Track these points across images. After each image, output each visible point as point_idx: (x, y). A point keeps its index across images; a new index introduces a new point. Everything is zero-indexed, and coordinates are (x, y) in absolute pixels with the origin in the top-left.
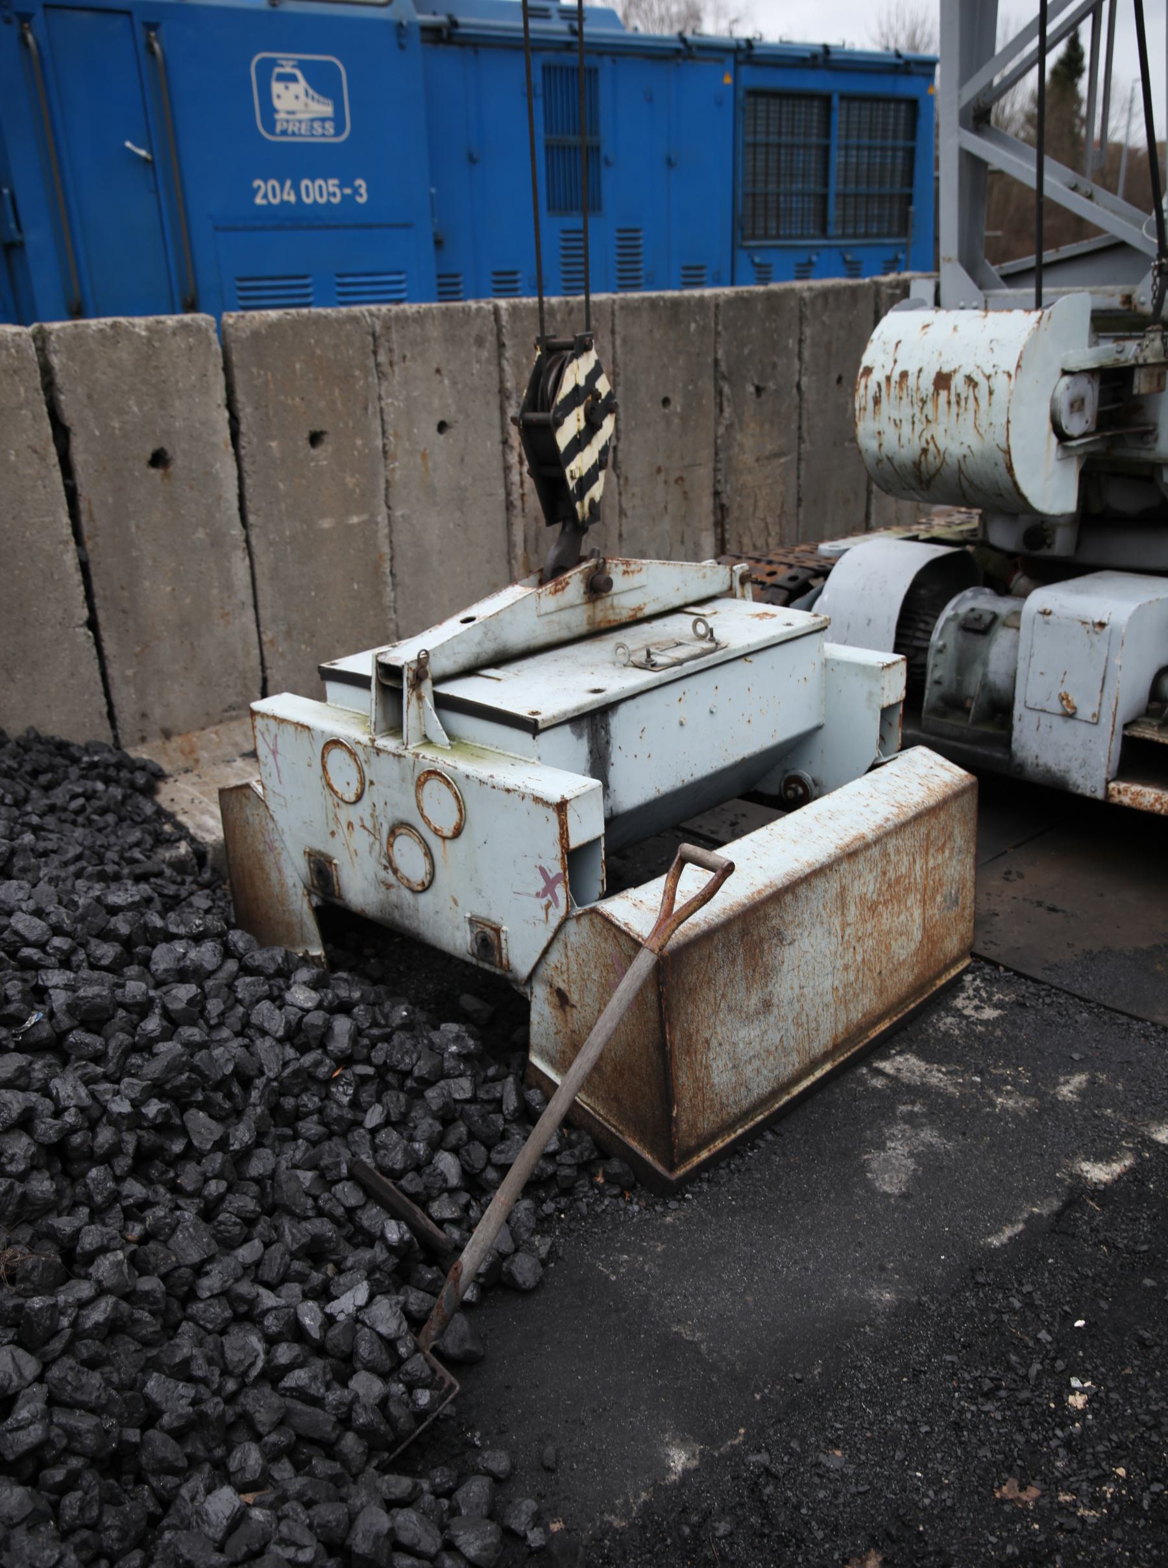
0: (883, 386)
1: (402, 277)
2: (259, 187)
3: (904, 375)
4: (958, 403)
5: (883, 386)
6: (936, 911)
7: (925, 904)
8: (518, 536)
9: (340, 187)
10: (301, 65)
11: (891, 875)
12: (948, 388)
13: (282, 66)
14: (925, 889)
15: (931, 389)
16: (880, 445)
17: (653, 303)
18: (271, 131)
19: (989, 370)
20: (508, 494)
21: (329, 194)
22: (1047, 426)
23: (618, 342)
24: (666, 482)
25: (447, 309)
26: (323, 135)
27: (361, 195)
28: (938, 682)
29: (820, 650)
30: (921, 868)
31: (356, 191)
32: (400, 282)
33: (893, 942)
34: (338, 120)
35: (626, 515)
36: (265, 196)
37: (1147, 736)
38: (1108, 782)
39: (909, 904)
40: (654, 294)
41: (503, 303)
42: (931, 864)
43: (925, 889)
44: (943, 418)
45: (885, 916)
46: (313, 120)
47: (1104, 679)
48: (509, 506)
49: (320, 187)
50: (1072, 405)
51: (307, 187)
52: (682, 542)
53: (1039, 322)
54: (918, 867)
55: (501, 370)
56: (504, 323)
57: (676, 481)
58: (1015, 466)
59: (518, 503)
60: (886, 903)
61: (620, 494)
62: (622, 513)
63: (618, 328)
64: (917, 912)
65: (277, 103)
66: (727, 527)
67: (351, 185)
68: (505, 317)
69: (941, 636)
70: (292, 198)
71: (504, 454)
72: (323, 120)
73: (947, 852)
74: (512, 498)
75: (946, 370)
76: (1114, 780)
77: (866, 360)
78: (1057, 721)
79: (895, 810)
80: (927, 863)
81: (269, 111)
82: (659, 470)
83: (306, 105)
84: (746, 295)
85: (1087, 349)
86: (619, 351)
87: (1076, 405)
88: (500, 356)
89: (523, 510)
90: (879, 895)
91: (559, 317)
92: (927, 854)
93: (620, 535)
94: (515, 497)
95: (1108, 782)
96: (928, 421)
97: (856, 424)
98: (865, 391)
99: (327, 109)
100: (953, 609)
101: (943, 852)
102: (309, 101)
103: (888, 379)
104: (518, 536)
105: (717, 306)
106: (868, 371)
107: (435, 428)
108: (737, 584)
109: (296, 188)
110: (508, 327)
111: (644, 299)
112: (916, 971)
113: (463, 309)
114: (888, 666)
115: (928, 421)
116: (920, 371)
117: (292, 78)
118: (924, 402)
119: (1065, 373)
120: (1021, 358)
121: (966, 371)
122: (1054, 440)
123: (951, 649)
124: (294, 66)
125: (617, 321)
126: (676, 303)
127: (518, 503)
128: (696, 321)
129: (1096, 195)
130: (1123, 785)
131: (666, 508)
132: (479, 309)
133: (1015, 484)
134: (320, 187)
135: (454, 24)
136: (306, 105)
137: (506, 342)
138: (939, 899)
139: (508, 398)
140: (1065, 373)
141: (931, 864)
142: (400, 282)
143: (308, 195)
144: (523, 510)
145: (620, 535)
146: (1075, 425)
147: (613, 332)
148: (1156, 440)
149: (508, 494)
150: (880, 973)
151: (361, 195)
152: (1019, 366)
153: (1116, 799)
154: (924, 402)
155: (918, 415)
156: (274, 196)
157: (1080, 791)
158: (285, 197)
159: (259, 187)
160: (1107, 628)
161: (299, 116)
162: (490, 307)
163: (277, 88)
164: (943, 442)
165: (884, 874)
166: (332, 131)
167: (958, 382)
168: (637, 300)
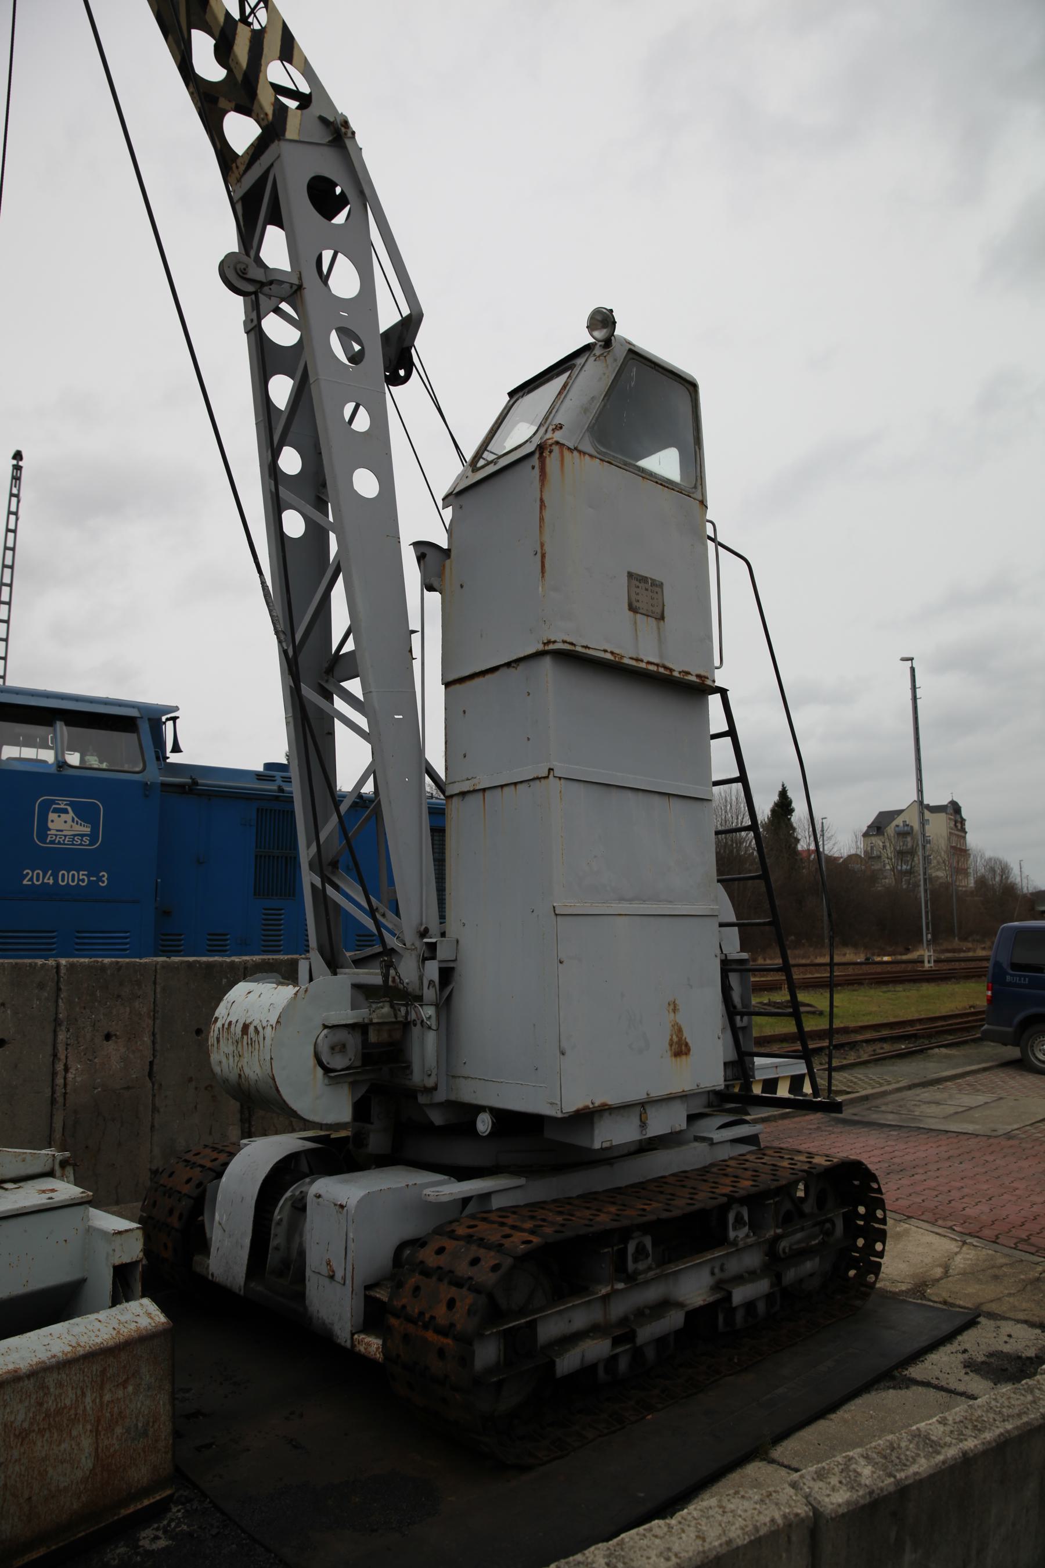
0: (221, 1030)
1: (128, 934)
2: (28, 874)
3: (230, 1023)
4: (251, 1044)
5: (221, 1030)
6: (115, 1441)
7: (98, 1432)
8: (58, 1125)
9: (88, 876)
10: (71, 804)
11: (50, 1404)
12: (247, 1034)
13: (59, 804)
14: (99, 1421)
15: (240, 1033)
16: (222, 1070)
17: (190, 965)
18: (44, 841)
19: (265, 1024)
20: (53, 1092)
21: (79, 880)
22: (312, 1061)
23: (158, 990)
24: (196, 1088)
25: (16, 964)
26: (81, 845)
27: (103, 882)
28: (277, 1248)
29: (86, 1218)
30: (94, 1401)
31: (100, 879)
32: (126, 938)
33: (50, 1470)
34: (93, 837)
35: (158, 1111)
36: (31, 879)
37: (378, 1296)
38: (353, 1334)
39: (74, 1433)
40: (191, 959)
41: (63, 961)
42: (107, 1397)
43: (99, 1421)
44: (246, 1055)
45: (39, 1444)
46: (75, 835)
47: (346, 1248)
48: (53, 1101)
49: (73, 875)
50: (332, 1048)
51: (63, 875)
52: (210, 1133)
53: (296, 994)
54: (88, 1400)
55: (57, 1006)
56: (62, 975)
57: (206, 1088)
58: (280, 1089)
59: (60, 1100)
60: (41, 1432)
61: (154, 1096)
62: (155, 1109)
63: (158, 981)
64: (86, 1443)
65: (50, 825)
66: (253, 1123)
67: (97, 876)
68: (63, 971)
69: (280, 1213)
70: (51, 882)
71: (53, 1063)
72: (83, 836)
73: (130, 1389)
74: (55, 1096)
75: (247, 1022)
76: (359, 1332)
77: (216, 1014)
78: (327, 1280)
79: (69, 1349)
80: (101, 1397)
81: (44, 828)
82: (190, 1080)
83: (71, 827)
84: (271, 961)
85: (349, 1011)
86: (158, 996)
87: (337, 1049)
88: (58, 996)
89: (65, 1105)
90: (31, 1424)
91: (109, 972)
92: (102, 1388)
93: (153, 1126)
94: (59, 1094)
95: (353, 1334)
96: (240, 1056)
97: (210, 1056)
98: (213, 1035)
99: (87, 830)
100: (292, 1192)
101: (125, 1388)
102: (74, 825)
103: (223, 1025)
104: (58, 1125)
105: (246, 968)
106: (217, 1019)
107: (194, 1033)
108: (57, 1167)
109: (55, 876)
110: (66, 977)
111: (182, 962)
112: (84, 1498)
113: (30, 964)
114: (120, 1233)
115: (240, 1056)
116: (237, 1022)
117: (66, 811)
118: (237, 1042)
119: (325, 1027)
120: (280, 1016)
121: (255, 1024)
122: (320, 1072)
123: (285, 1223)
124: (66, 805)
125: (158, 976)
126: (209, 966)
127: (60, 1100)
128: (227, 978)
129: (387, 915)
130: (362, 1336)
131: (196, 1107)
132: (43, 965)
133: (284, 1101)
134: (73, 875)
135: (195, 783)
136: (71, 827)
137: (62, 987)
138: (119, 1430)
139: (60, 1025)
140: (325, 1027)
141: (107, 1397)
142: (126, 938)
143: (63, 881)
144: (65, 1105)
145: (153, 1126)
146: (338, 1062)
147: (155, 983)
148: (412, 1073)
149: (53, 1092)
150: (30, 1498)
151: (103, 882)
152: (278, 1022)
153: (362, 1348)
154: (237, 1042)
155: (235, 1051)
156: (38, 880)
157: (339, 1341)
158: (46, 881)
159: (28, 874)
160: (345, 1209)
161: (64, 833)
162: (54, 963)
163: (52, 816)
164: (247, 1071)
165: (41, 1404)
166: (88, 842)
167: (251, 1029)
168: (176, 963)
